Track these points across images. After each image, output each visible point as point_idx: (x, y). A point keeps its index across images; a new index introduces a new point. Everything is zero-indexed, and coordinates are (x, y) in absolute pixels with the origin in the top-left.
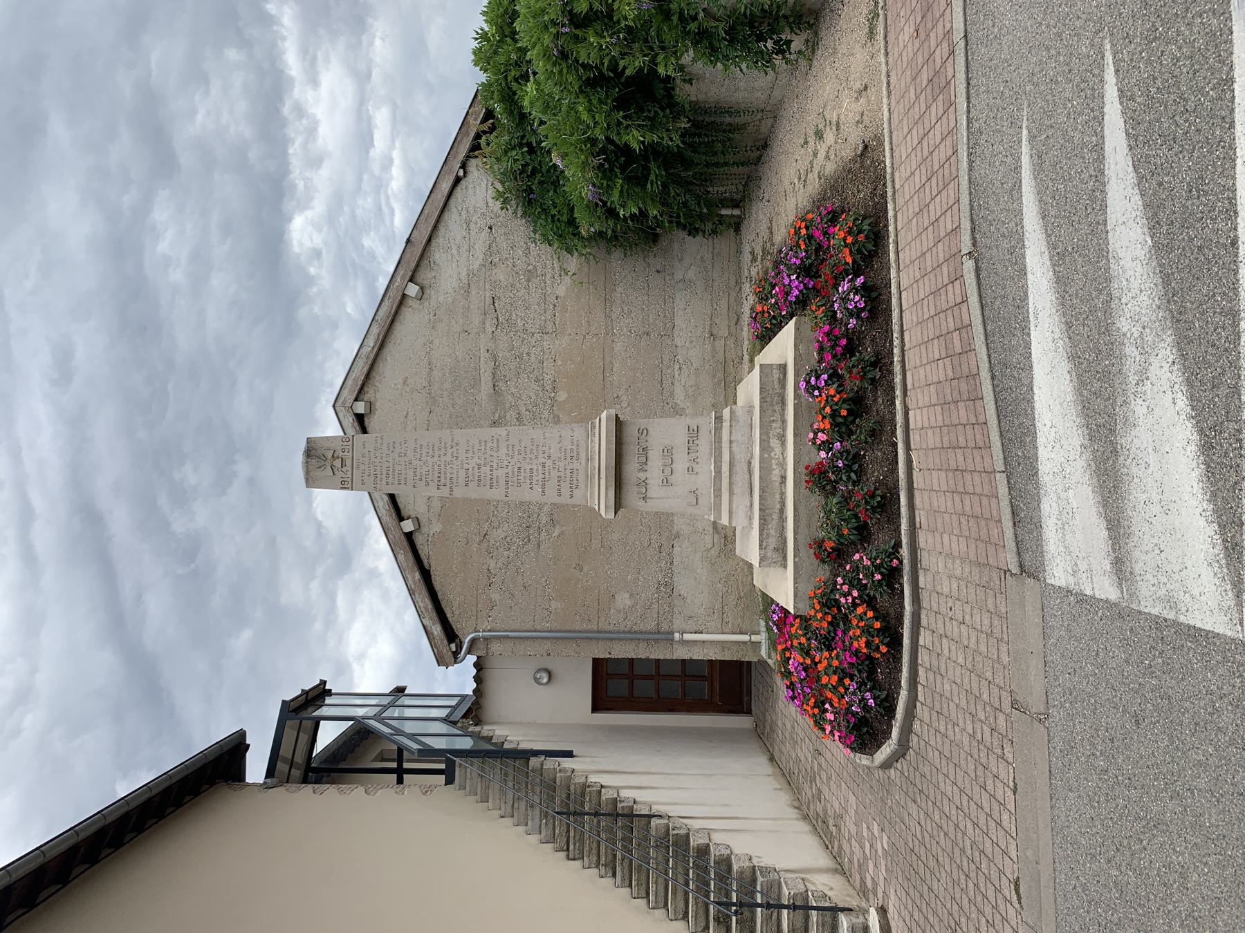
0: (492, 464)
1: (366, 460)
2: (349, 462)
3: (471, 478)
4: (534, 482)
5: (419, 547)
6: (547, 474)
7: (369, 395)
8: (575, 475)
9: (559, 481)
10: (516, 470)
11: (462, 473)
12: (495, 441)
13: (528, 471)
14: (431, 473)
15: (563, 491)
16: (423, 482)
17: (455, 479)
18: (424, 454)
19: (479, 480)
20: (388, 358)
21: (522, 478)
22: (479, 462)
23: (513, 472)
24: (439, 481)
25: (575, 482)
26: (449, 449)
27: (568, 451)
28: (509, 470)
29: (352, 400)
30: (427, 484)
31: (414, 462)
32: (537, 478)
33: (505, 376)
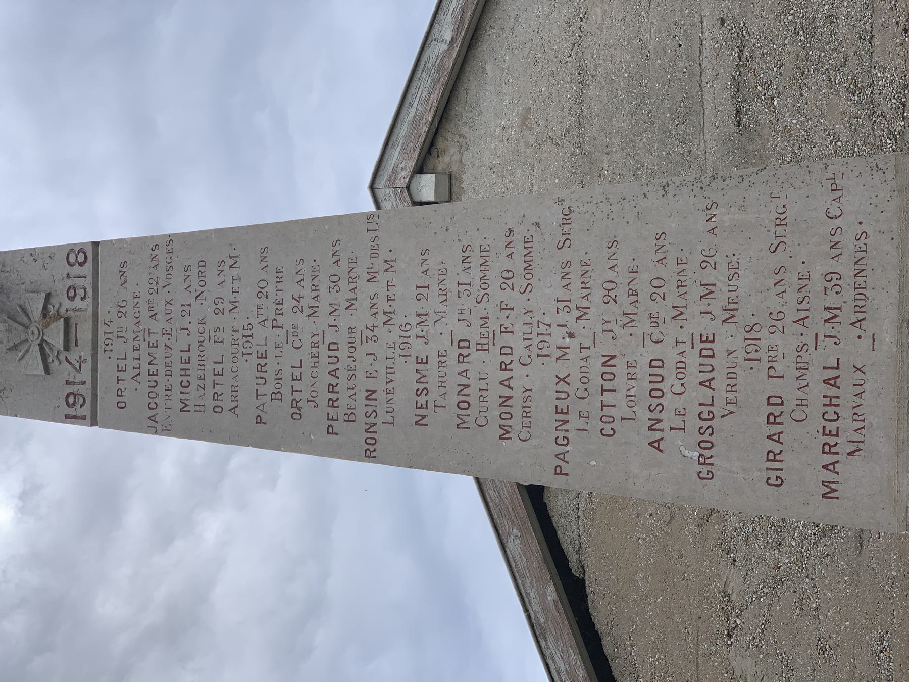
0: (508, 339)
1: (129, 322)
2: (84, 334)
3: (434, 395)
4: (669, 419)
5: (558, 522)
6: (720, 384)
7: (447, 159)
8: (846, 394)
9: (772, 420)
10: (596, 366)
11: (406, 374)
12: (519, 249)
13: (643, 370)
14: (307, 371)
15: (790, 460)
16: (285, 408)
17: (381, 396)
18: (288, 304)
19: (463, 405)
20: (489, 67)
21: (618, 398)
22: (461, 331)
23: (585, 373)
24: (332, 403)
25: (847, 424)
26: (361, 283)
27: (817, 284)
28: (571, 367)
29: (406, 173)
30: (297, 413)
31: (259, 333)
32: (679, 403)
33: (767, 85)
